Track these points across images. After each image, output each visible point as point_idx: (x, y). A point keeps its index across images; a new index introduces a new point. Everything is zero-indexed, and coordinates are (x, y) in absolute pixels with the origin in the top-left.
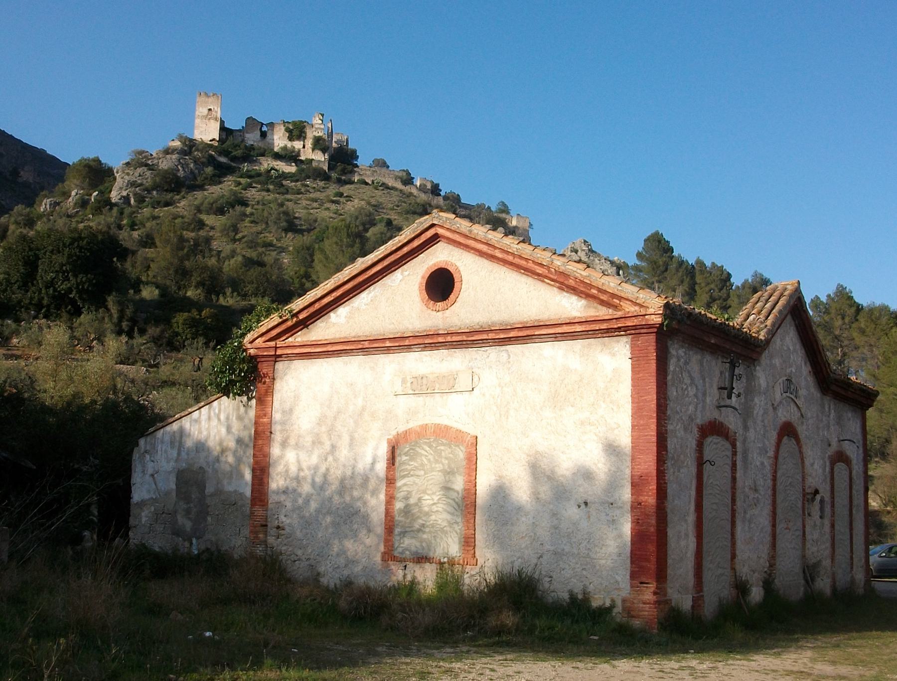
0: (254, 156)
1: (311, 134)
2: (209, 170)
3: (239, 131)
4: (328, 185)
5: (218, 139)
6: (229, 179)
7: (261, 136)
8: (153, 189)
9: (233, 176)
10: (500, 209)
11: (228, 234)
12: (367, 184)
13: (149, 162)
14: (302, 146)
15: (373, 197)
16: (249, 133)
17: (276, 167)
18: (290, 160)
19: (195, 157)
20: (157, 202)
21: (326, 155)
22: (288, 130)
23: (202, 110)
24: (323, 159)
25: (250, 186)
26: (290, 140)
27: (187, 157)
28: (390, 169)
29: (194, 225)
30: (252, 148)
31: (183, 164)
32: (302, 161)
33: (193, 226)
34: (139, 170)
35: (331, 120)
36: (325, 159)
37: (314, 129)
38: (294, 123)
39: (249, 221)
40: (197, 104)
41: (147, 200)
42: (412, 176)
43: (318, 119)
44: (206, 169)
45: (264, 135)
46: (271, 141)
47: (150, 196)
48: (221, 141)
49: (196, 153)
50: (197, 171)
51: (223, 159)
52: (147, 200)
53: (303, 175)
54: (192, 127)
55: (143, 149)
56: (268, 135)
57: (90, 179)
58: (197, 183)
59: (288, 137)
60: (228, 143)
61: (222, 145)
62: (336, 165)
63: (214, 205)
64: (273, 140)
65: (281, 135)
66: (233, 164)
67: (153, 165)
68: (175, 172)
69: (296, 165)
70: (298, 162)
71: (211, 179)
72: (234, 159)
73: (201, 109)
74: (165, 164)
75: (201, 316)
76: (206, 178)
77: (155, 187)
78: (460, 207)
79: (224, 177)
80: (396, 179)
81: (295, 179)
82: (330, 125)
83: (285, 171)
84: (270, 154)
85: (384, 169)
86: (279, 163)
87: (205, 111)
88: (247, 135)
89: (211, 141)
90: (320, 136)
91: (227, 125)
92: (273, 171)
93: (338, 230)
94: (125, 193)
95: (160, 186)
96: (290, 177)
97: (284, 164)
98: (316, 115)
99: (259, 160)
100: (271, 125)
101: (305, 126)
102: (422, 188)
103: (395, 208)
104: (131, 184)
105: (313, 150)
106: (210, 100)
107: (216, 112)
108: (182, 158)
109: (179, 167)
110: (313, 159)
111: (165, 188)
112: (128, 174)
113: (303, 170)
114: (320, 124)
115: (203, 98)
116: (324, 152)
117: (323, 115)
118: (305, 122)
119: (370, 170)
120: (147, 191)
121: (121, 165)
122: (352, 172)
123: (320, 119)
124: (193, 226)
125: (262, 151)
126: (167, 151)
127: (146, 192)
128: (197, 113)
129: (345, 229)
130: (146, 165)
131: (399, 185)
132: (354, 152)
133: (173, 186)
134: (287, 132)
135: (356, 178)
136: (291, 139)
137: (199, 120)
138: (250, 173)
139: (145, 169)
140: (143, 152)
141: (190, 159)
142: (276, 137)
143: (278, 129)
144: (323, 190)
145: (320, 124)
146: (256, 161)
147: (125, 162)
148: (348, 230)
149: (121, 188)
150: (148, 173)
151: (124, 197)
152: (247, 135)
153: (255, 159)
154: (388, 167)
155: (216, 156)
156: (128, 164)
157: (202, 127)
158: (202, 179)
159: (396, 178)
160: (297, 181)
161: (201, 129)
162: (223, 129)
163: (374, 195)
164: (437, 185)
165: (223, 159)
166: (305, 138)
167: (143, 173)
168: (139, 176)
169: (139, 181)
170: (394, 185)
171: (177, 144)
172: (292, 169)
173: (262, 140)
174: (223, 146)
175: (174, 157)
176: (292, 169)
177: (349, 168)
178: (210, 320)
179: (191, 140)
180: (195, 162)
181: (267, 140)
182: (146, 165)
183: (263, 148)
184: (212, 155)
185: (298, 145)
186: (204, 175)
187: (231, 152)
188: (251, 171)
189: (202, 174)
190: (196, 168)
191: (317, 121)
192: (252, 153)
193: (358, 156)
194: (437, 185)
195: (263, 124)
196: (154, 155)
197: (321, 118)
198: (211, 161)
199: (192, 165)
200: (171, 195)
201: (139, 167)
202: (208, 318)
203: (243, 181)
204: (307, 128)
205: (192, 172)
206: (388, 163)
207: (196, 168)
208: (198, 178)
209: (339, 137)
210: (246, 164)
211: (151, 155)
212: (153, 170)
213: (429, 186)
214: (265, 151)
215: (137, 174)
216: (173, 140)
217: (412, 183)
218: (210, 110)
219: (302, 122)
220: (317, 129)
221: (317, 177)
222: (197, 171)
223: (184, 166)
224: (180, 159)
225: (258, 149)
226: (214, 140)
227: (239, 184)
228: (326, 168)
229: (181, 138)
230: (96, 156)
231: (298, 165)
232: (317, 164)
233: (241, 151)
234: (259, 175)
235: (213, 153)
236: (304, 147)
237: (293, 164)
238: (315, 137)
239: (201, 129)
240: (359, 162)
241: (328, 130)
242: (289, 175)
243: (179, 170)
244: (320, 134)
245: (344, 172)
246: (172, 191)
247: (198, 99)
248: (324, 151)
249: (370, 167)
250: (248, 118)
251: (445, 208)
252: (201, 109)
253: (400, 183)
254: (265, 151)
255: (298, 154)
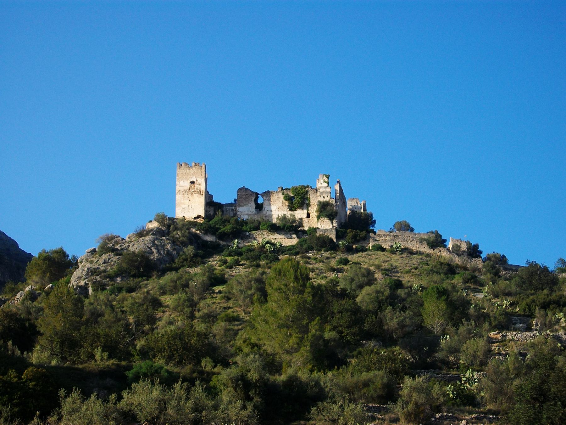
0: (246, 231)
1: (315, 200)
2: (190, 250)
3: (231, 205)
4: (333, 255)
5: (204, 216)
6: (216, 259)
7: (256, 208)
8: (117, 275)
9: (220, 255)
10: (559, 269)
11: (182, 311)
12: (383, 250)
13: (118, 247)
14: (306, 215)
15: (387, 261)
16: (243, 206)
17: (273, 241)
18: (290, 231)
19: (173, 237)
20: (117, 288)
21: (334, 222)
22: (289, 199)
23: (182, 184)
24: (331, 227)
25: (237, 263)
26: (291, 210)
27: (164, 238)
28: (415, 232)
29: (147, 306)
30: (245, 222)
31: (157, 246)
32: (304, 232)
33: (145, 307)
34: (105, 257)
35: (339, 182)
36: (333, 227)
37: (319, 194)
38: (295, 190)
39: (221, 297)
40: (177, 177)
41: (108, 288)
42: (443, 238)
43: (322, 181)
44: (185, 249)
45: (259, 207)
46: (268, 213)
47: (112, 283)
48: (208, 217)
49: (175, 233)
50: (174, 253)
51: (209, 238)
52: (108, 288)
53: (305, 246)
54: (173, 204)
55: (114, 235)
56: (264, 206)
57: (51, 272)
58: (174, 265)
59: (289, 206)
60: (216, 218)
61: (209, 221)
62: (346, 232)
63: (178, 282)
64: (271, 211)
65: (280, 204)
66: (222, 243)
67: (122, 249)
68: (147, 255)
69: (298, 237)
70: (300, 233)
71: (191, 260)
72: (223, 236)
73: (181, 182)
74: (137, 247)
75: (20, 378)
76: (186, 260)
77: (120, 273)
78: (506, 269)
79: (209, 258)
80: (421, 242)
81: (293, 251)
82: (337, 187)
83: (284, 244)
84: (266, 226)
85: (407, 233)
86: (276, 236)
87: (187, 185)
88: (240, 209)
89: (195, 218)
90: (326, 201)
91: (215, 200)
92: (267, 245)
93: (282, 273)
94: (82, 283)
95: (126, 272)
96: (290, 250)
97: (283, 237)
98: (320, 177)
99: (253, 235)
100: (268, 194)
101: (307, 191)
102: (456, 250)
103: (413, 270)
104: (92, 271)
105: (319, 218)
106: (192, 171)
107: (200, 184)
108: (157, 239)
109: (153, 248)
110: (318, 228)
111: (133, 273)
112: (91, 262)
113: (305, 241)
114: (325, 187)
115: (184, 170)
116: (331, 220)
117: (328, 177)
118: (308, 186)
119: (389, 236)
120: (108, 277)
121: (86, 254)
122: (366, 239)
123: (325, 182)
124: (145, 307)
125: (256, 224)
126: (141, 234)
127: (108, 279)
128: (178, 188)
129: (292, 271)
130: (113, 250)
131: (426, 249)
132: (370, 216)
133: (142, 270)
134: (286, 200)
135: (371, 244)
136: (292, 208)
137: (180, 196)
138: (240, 250)
139: (112, 255)
140: (113, 238)
141: (167, 239)
142: (273, 208)
143: (275, 198)
144: (327, 261)
145: (325, 187)
146: (249, 237)
147: (90, 250)
148: (296, 271)
149: (79, 278)
150: (115, 258)
151: (81, 287)
152: (240, 209)
153: (248, 234)
154: (412, 230)
155: (201, 235)
156: (94, 251)
157: (184, 204)
158: (181, 260)
159: (421, 241)
160: (297, 254)
161: (183, 206)
162: (210, 203)
163: (389, 259)
164: (476, 246)
165: (209, 238)
166: (308, 205)
167: (109, 259)
168: (104, 263)
169: (102, 269)
170: (419, 249)
171: (155, 225)
172: (293, 241)
173: (258, 214)
174: (211, 222)
175: (147, 238)
176: (293, 241)
177: (363, 234)
178: (33, 383)
179: (173, 220)
180: (174, 242)
181: (264, 212)
182: (113, 250)
183: (257, 221)
184: (196, 235)
185: (300, 214)
186: (184, 256)
187: (220, 229)
188: (242, 248)
189: (182, 255)
190: (175, 249)
191: (321, 184)
192: (244, 228)
193: (375, 221)
194: (476, 246)
195: (257, 194)
196: (127, 239)
197: (326, 180)
198: (194, 239)
199: (169, 247)
200: (136, 280)
201: (105, 253)
202: (31, 380)
203: (229, 259)
204: (310, 193)
205: (168, 253)
206: (412, 226)
207: (175, 249)
208: (176, 261)
209: (354, 203)
210: (236, 240)
211: (123, 239)
212: (120, 255)
213: (464, 247)
214: (260, 223)
215: (101, 261)
216: (151, 221)
217: (445, 246)
218: (192, 182)
219: (303, 187)
220: (322, 193)
221: (322, 247)
222: (174, 253)
223: (160, 248)
224: (154, 241)
225: (252, 223)
226: (199, 217)
227: (225, 262)
228: (333, 236)
229: (161, 219)
230: (59, 247)
231: (300, 236)
232: (321, 233)
233: (231, 225)
234: (251, 250)
235: (198, 232)
236: (308, 216)
237: (294, 236)
238: (320, 202)
239: (183, 206)
240: (378, 228)
241: (336, 193)
242: (288, 248)
243: (152, 253)
244: (327, 199)
245: (356, 239)
246: (141, 275)
247: (178, 171)
248: (331, 217)
249: (390, 232)
250: (240, 189)
251: (484, 269)
252: (181, 182)
253: (427, 247)
254: (260, 223)
255: (301, 224)
